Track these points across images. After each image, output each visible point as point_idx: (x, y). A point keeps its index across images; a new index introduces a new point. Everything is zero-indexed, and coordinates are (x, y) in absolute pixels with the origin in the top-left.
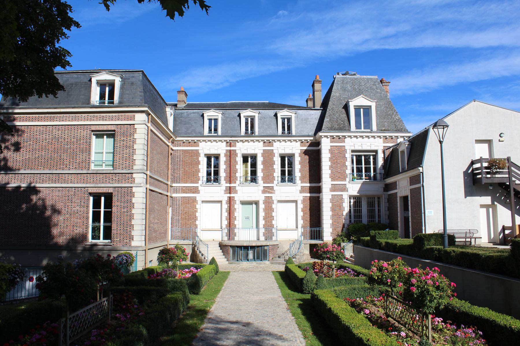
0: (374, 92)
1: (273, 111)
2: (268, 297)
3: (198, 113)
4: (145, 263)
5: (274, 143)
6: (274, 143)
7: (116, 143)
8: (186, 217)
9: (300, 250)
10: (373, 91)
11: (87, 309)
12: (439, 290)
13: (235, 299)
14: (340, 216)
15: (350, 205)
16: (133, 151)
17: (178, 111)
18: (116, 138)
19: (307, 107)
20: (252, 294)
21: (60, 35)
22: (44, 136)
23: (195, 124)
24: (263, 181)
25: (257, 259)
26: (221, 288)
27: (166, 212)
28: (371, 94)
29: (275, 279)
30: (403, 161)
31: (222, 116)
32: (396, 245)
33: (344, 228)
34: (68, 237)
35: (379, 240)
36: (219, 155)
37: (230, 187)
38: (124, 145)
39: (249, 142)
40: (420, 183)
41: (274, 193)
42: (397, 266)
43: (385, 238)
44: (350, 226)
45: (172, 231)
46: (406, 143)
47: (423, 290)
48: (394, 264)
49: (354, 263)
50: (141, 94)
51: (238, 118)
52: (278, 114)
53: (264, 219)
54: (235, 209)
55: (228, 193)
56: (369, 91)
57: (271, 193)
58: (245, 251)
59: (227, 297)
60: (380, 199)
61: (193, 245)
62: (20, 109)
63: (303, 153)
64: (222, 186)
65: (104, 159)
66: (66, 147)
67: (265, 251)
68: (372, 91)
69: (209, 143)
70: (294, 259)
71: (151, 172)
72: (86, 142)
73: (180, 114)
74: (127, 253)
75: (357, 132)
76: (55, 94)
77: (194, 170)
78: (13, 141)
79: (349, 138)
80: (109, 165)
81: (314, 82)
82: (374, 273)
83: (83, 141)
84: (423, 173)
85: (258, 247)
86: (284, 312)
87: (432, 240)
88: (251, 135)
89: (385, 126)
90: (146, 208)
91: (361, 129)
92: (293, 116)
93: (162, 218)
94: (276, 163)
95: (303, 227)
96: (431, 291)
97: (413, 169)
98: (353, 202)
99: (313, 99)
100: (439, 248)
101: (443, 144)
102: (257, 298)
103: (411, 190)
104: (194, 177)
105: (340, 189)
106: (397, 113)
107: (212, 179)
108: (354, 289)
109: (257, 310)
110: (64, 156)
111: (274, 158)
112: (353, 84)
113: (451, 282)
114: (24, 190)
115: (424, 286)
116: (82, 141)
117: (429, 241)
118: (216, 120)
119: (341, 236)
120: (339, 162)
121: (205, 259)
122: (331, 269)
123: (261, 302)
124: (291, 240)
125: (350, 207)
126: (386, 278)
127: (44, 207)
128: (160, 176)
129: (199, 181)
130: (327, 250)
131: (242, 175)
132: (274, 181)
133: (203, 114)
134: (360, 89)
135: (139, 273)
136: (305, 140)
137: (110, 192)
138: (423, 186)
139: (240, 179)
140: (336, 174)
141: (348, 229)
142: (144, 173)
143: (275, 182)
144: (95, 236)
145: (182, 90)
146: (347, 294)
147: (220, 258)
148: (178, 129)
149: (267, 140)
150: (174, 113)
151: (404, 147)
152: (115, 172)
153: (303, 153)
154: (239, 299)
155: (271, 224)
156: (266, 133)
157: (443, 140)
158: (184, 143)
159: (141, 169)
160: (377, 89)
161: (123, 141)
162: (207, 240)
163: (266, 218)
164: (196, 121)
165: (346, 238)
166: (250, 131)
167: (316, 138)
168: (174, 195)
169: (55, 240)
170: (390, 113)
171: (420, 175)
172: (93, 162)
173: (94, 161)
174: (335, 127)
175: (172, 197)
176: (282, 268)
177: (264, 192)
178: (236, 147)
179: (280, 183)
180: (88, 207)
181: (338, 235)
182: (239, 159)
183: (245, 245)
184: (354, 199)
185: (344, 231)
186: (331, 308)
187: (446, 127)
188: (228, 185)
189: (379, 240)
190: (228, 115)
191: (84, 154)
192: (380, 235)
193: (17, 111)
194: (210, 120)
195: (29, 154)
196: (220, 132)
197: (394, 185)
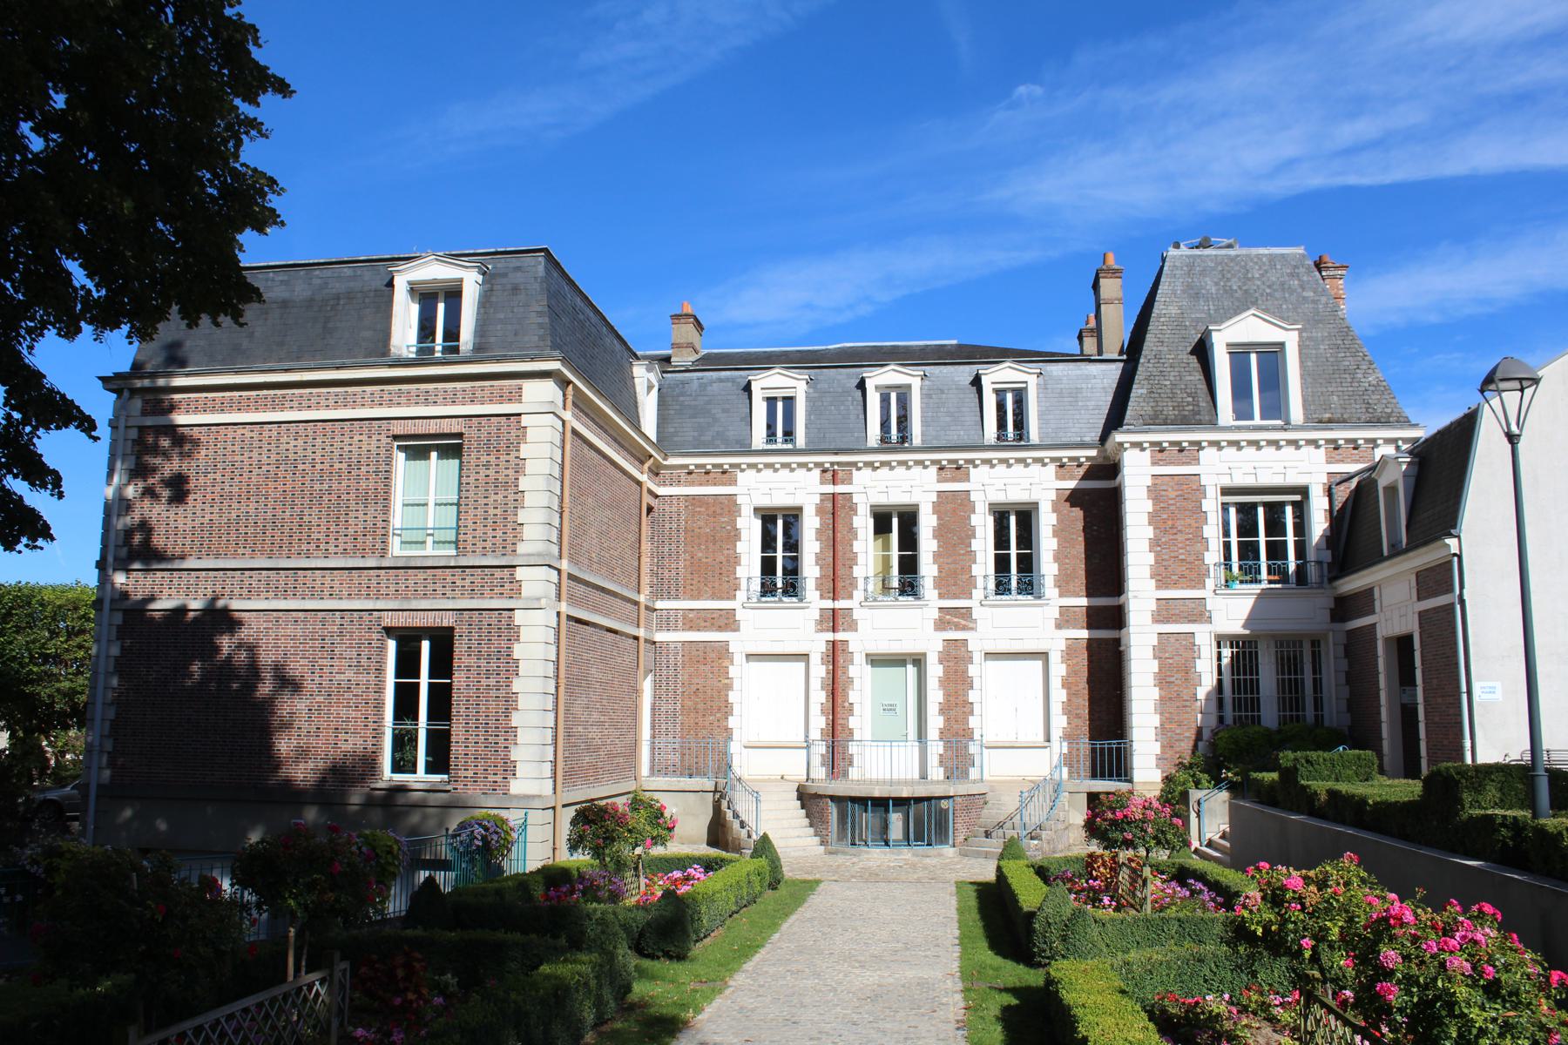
0: (1294, 298)
1: (967, 368)
2: (910, 974)
3: (733, 380)
4: (554, 849)
5: (972, 470)
6: (972, 470)
7: (464, 473)
8: (696, 703)
9: (1055, 811)
10: (1291, 294)
11: (228, 1012)
12: (1499, 1001)
13: (796, 979)
14: (1188, 703)
15: (1219, 667)
16: (516, 497)
17: (674, 375)
18: (465, 459)
19: (1082, 354)
20: (857, 965)
21: (246, 127)
22: (255, 455)
23: (725, 415)
24: (937, 591)
25: (915, 841)
26: (765, 939)
27: (636, 691)
28: (1284, 306)
29: (957, 909)
30: (1392, 519)
31: (809, 387)
32: (1363, 801)
33: (1201, 740)
34: (321, 765)
35: (1310, 783)
36: (800, 509)
37: (833, 610)
38: (488, 480)
39: (892, 468)
40: (1450, 589)
41: (972, 629)
42: (1342, 889)
43: (1330, 777)
44: (1220, 735)
45: (653, 749)
46: (1400, 460)
47: (1430, 994)
48: (1327, 881)
49: (1228, 859)
50: (540, 320)
51: (859, 393)
52: (983, 378)
53: (942, 711)
54: (851, 681)
55: (828, 631)
56: (1277, 295)
57: (964, 628)
58: (878, 814)
59: (772, 970)
60: (1319, 647)
61: (715, 791)
62: (187, 375)
63: (1066, 501)
64: (808, 608)
65: (430, 525)
66: (317, 487)
67: (941, 814)
68: (1287, 295)
69: (768, 473)
70: (1036, 842)
71: (572, 559)
72: (377, 472)
73: (678, 385)
74: (489, 815)
75: (1239, 428)
76: (237, 316)
77: (722, 558)
78: (167, 473)
79: (1214, 450)
80: (444, 542)
81: (1097, 275)
82: (1251, 912)
83: (367, 469)
84: (1460, 557)
85: (919, 800)
86: (941, 1037)
87: (1488, 788)
88: (897, 445)
89: (1331, 408)
90: (558, 676)
91: (1251, 418)
92: (1032, 382)
93: (616, 706)
94: (979, 532)
95: (1068, 736)
96: (1463, 1005)
97: (1425, 543)
98: (1230, 655)
99: (1098, 332)
100: (1515, 818)
101: (1521, 446)
102: (870, 978)
103: (1422, 615)
104: (721, 580)
105: (1186, 615)
106: (1371, 363)
107: (780, 585)
108: (1199, 961)
109: (855, 1024)
110: (312, 516)
111: (972, 516)
112: (1223, 276)
113: (1551, 968)
114: (195, 618)
115: (1435, 979)
116: (364, 469)
117: (1478, 792)
118: (789, 401)
119: (1191, 766)
120: (1179, 528)
121: (749, 836)
122: (1140, 881)
123: (876, 996)
124: (1030, 778)
125: (1220, 672)
126: (1295, 931)
127: (254, 670)
128: (611, 575)
129: (738, 593)
130: (1126, 816)
131: (871, 573)
132: (974, 591)
133: (749, 383)
134: (1246, 291)
135: (510, 883)
136: (1071, 459)
137: (445, 624)
138: (1462, 602)
139: (866, 584)
140: (1173, 566)
141: (1213, 745)
142: (549, 566)
143: (978, 594)
144: (403, 763)
145: (685, 312)
146: (1172, 976)
147: (798, 837)
148: (672, 430)
149: (950, 461)
150: (659, 381)
151: (1396, 474)
152: (463, 562)
153: (1066, 501)
154: (809, 982)
155: (966, 727)
156: (947, 438)
157: (1521, 431)
158: (690, 473)
159: (539, 555)
160: (1303, 289)
161: (487, 465)
162: (766, 777)
163: (949, 709)
164: (728, 406)
165: (1206, 776)
166: (897, 438)
167: (1106, 451)
168: (660, 637)
169: (283, 772)
170: (1347, 363)
171: (1450, 563)
172: (396, 532)
173: (402, 529)
174: (1165, 413)
175: (655, 643)
176: (990, 875)
177: (941, 625)
178: (851, 484)
179: (991, 598)
180: (380, 671)
181: (1180, 763)
182: (864, 523)
183: (877, 794)
184: (1232, 647)
185: (1198, 753)
186: (1087, 1037)
187: (1530, 383)
188: (829, 604)
189: (1310, 783)
190: (826, 386)
191: (371, 511)
192: (1312, 765)
193: (179, 382)
194: (771, 401)
195: (212, 510)
196: (801, 439)
197: (1363, 602)
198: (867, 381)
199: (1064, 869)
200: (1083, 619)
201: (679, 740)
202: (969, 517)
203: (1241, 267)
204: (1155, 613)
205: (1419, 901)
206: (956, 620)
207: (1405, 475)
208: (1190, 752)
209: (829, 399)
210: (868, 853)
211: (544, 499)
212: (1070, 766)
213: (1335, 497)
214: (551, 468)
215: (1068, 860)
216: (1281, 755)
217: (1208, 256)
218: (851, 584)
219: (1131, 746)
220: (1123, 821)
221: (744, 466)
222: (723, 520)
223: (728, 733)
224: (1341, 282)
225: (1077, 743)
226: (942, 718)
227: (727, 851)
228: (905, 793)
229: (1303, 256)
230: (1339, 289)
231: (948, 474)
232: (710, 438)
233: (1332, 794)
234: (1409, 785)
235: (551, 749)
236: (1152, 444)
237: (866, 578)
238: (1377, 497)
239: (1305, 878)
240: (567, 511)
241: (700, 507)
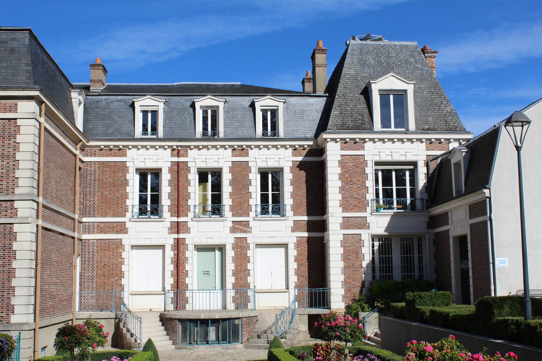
0: (411, 67)
3: (124, 101)
4: (34, 352)
5: (250, 151)
8: (105, 272)
10: (410, 66)
14: (358, 269)
15: (373, 251)
16: (14, 163)
19: (304, 92)
27: (72, 266)
32: (447, 315)
35: (421, 307)
37: (178, 222)
39: (208, 149)
40: (485, 214)
41: (249, 232)
42: (449, 350)
44: (374, 284)
45: (80, 296)
46: (462, 150)
48: (443, 347)
50: (27, 68)
51: (191, 110)
53: (234, 274)
54: (187, 259)
55: (175, 233)
57: (245, 232)
60: (421, 241)
61: (116, 318)
63: (297, 167)
64: (164, 221)
67: (235, 328)
69: (143, 151)
70: (284, 340)
71: (45, 198)
73: (94, 103)
75: (384, 132)
77: (118, 195)
79: (371, 143)
84: (490, 198)
87: (505, 307)
89: (428, 123)
91: (390, 127)
92: (281, 106)
94: (253, 183)
95: (297, 286)
97: (474, 191)
98: (378, 245)
99: (313, 80)
100: (517, 320)
101: (522, 152)
103: (471, 225)
105: (357, 225)
106: (448, 101)
107: (149, 209)
117: (501, 309)
118: (155, 113)
119: (360, 300)
120: (354, 182)
121: (136, 341)
122: (343, 356)
125: (373, 254)
128: (62, 205)
130: (336, 324)
131: (197, 203)
132: (250, 213)
133: (133, 103)
136: (300, 146)
138: (491, 220)
141: (370, 290)
142: (33, 200)
143: (252, 214)
145: (97, 63)
148: (91, 127)
149: (238, 146)
150: (84, 100)
151: (459, 157)
153: (297, 167)
155: (246, 283)
157: (522, 145)
158: (101, 150)
159: (27, 194)
160: (416, 63)
162: (142, 310)
163: (238, 273)
164: (121, 115)
167: (318, 142)
168: (84, 237)
170: (437, 101)
171: (485, 201)
174: (348, 124)
175: (82, 240)
177: (233, 230)
178: (187, 157)
179: (259, 216)
181: (354, 299)
182: (193, 177)
183: (202, 317)
184: (379, 241)
185: (363, 294)
188: (175, 219)
189: (421, 307)
192: (422, 298)
194: (145, 113)
197: (443, 219)
198: (196, 103)
199: (301, 352)
200: (305, 227)
201: (94, 292)
203: (386, 51)
204: (342, 224)
205: (485, 353)
206: (241, 227)
207: (465, 158)
208: (359, 293)
209: (175, 112)
210: (198, 348)
211: (30, 165)
212: (299, 302)
213: (430, 167)
214: (34, 148)
215: (303, 348)
216: (407, 294)
217: (370, 44)
218: (187, 209)
219: (330, 291)
220: (335, 326)
221: (130, 147)
222: (119, 175)
223: (122, 288)
224: (434, 59)
225: (302, 290)
226: (234, 278)
227: (123, 349)
228: (217, 317)
229: (417, 46)
230: (433, 63)
231: (238, 152)
232: (112, 131)
233: (432, 312)
234: (468, 307)
235: (33, 298)
236: (341, 139)
237: (195, 206)
238: (451, 168)
239: (434, 347)
240: (42, 170)
241: (107, 168)
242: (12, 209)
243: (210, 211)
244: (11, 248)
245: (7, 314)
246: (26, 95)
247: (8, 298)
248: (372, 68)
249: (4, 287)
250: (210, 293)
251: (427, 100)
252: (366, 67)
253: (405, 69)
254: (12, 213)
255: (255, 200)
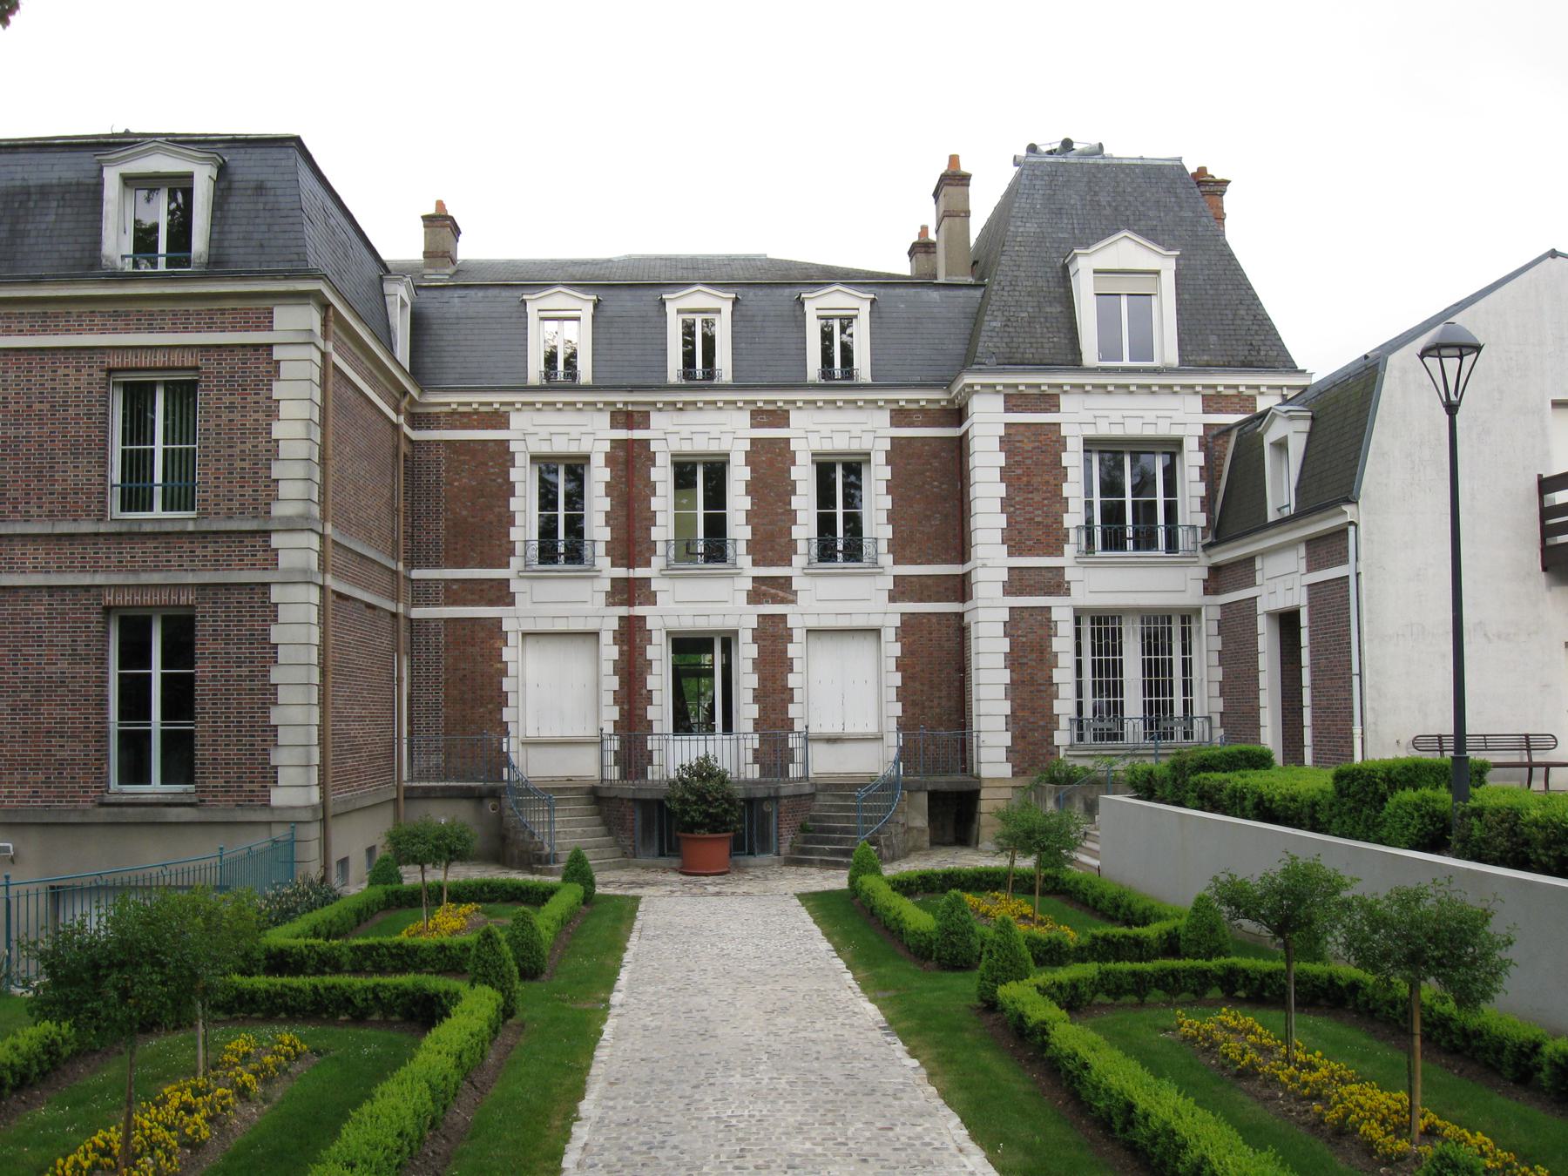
14: (1042, 688)
57: (783, 601)
75: (1106, 370)
77: (491, 517)
107: (561, 549)
112: (1090, 187)
116: (71, 411)
143: (799, 561)
160: (1181, 208)
168: (418, 613)
170: (1229, 297)
177: (755, 597)
180: (103, 660)
182: (662, 475)
188: (621, 572)
202: (789, 471)
206: (773, 591)
214: (311, 412)
223: (504, 729)
242: (266, 551)
243: (701, 554)
244: (266, 639)
245: (262, 787)
246: (292, 289)
247: (263, 750)
248: (1078, 219)
249: (254, 726)
250: (706, 740)
251: (1206, 294)
252: (1064, 216)
253: (1155, 223)
254: (267, 560)
255: (805, 529)
